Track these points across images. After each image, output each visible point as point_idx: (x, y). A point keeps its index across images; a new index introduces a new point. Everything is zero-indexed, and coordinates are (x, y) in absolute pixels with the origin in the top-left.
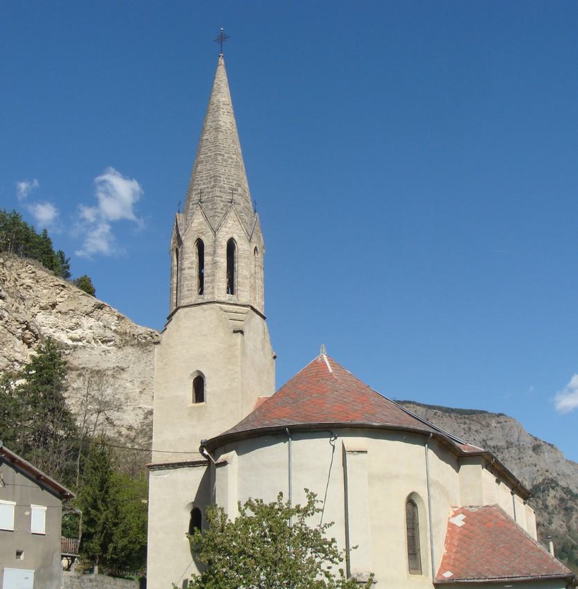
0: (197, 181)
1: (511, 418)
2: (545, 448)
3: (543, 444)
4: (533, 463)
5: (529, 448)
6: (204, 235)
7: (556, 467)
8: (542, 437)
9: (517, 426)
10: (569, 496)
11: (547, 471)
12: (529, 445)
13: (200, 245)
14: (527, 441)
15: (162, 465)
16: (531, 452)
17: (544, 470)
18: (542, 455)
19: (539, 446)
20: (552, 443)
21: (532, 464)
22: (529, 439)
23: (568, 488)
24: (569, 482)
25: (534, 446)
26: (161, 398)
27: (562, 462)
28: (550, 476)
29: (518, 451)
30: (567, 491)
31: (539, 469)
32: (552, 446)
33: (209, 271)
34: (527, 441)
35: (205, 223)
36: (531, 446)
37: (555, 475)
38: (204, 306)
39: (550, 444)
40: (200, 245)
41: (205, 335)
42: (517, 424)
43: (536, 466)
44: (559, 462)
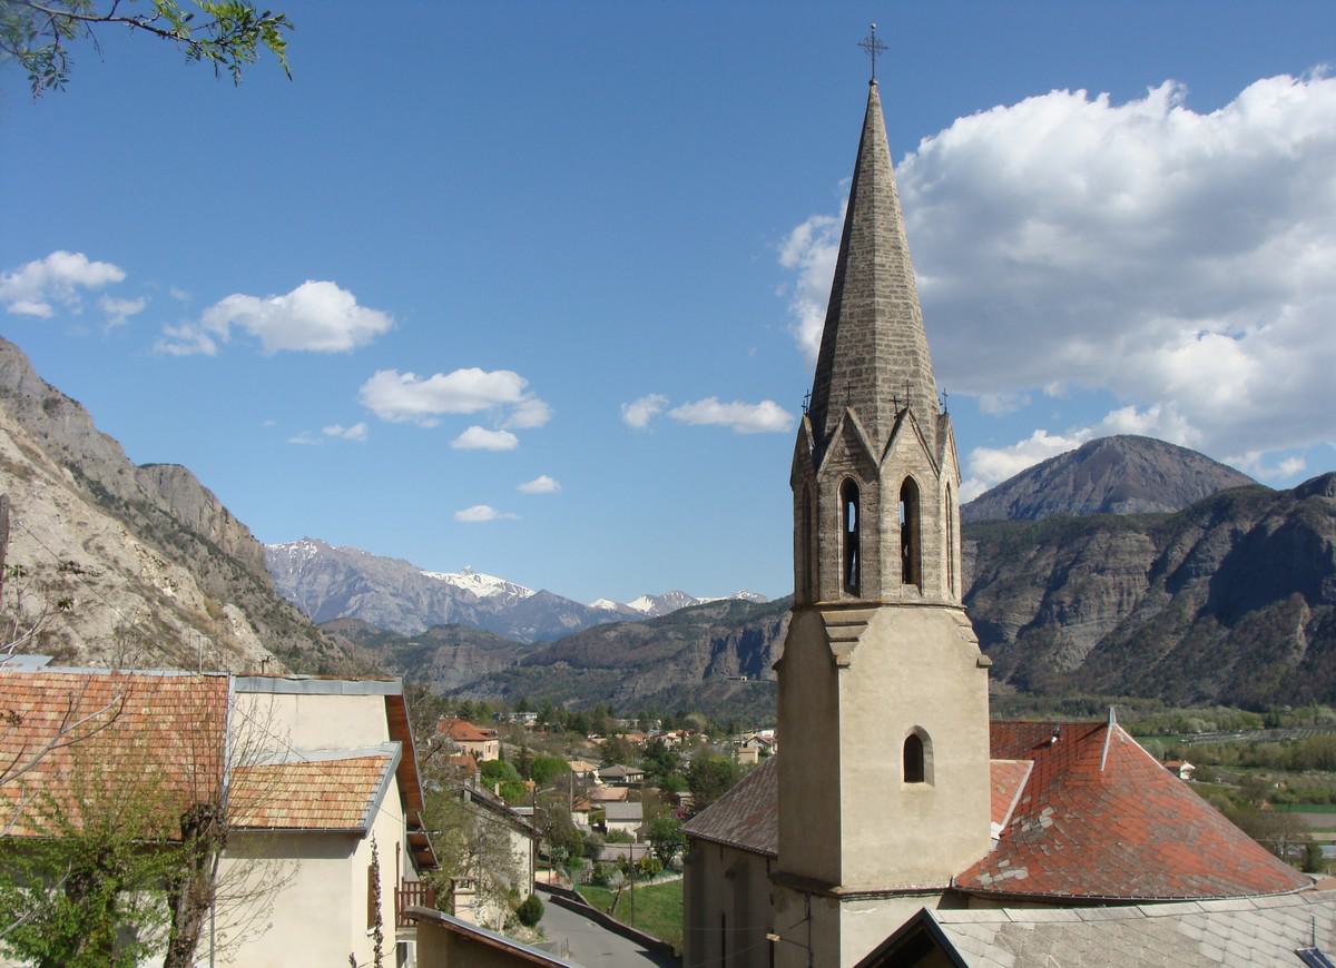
0: (881, 351)
1: (10, 343)
2: (67, 407)
3: (62, 399)
4: (42, 430)
5: (37, 402)
6: (919, 472)
7: (82, 443)
8: (65, 387)
9: (20, 360)
10: (100, 497)
11: (65, 448)
12: (38, 397)
13: (909, 491)
14: (36, 391)
15: (865, 893)
16: (40, 411)
17: (61, 446)
18: (59, 418)
19: (56, 402)
20: (76, 399)
21: (40, 433)
22: (38, 387)
23: (98, 483)
24: (101, 473)
25: (47, 401)
26: (855, 770)
27: (94, 436)
28: (70, 459)
29: (16, 405)
30: (97, 489)
31: (52, 443)
32: (76, 404)
33: (931, 545)
34: (36, 391)
35: (921, 450)
36: (41, 401)
37: (79, 457)
38: (926, 609)
39: (72, 401)
40: (909, 491)
41: (929, 664)
42: (21, 356)
43: (46, 437)
44: (88, 434)
